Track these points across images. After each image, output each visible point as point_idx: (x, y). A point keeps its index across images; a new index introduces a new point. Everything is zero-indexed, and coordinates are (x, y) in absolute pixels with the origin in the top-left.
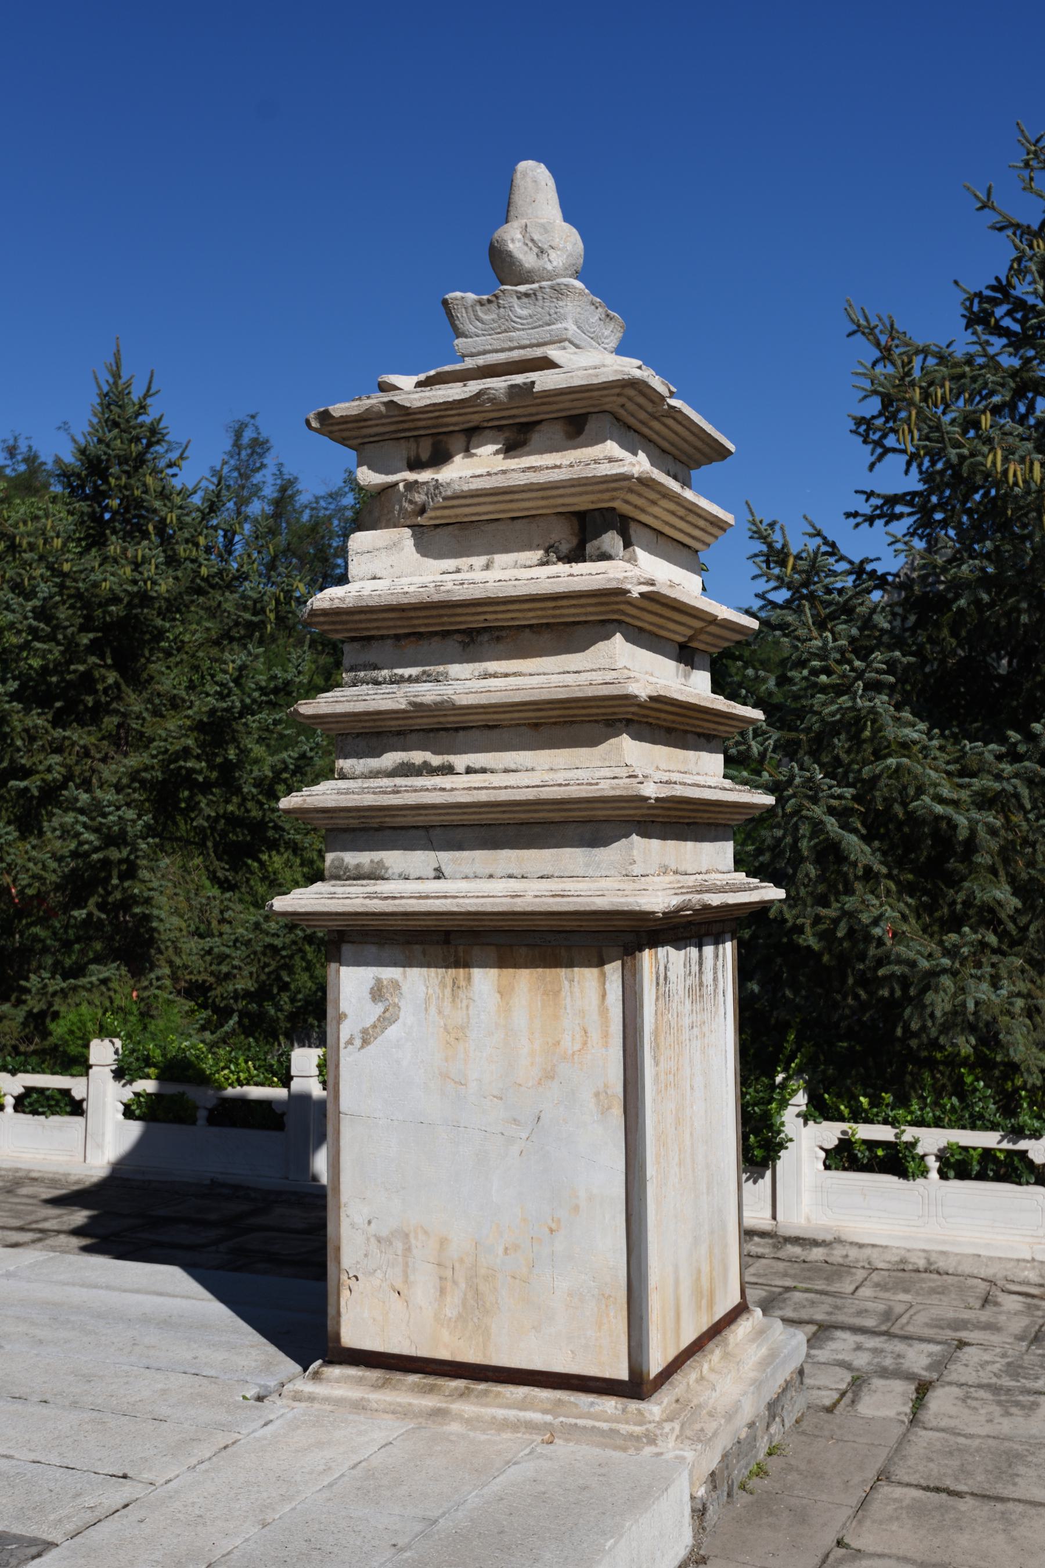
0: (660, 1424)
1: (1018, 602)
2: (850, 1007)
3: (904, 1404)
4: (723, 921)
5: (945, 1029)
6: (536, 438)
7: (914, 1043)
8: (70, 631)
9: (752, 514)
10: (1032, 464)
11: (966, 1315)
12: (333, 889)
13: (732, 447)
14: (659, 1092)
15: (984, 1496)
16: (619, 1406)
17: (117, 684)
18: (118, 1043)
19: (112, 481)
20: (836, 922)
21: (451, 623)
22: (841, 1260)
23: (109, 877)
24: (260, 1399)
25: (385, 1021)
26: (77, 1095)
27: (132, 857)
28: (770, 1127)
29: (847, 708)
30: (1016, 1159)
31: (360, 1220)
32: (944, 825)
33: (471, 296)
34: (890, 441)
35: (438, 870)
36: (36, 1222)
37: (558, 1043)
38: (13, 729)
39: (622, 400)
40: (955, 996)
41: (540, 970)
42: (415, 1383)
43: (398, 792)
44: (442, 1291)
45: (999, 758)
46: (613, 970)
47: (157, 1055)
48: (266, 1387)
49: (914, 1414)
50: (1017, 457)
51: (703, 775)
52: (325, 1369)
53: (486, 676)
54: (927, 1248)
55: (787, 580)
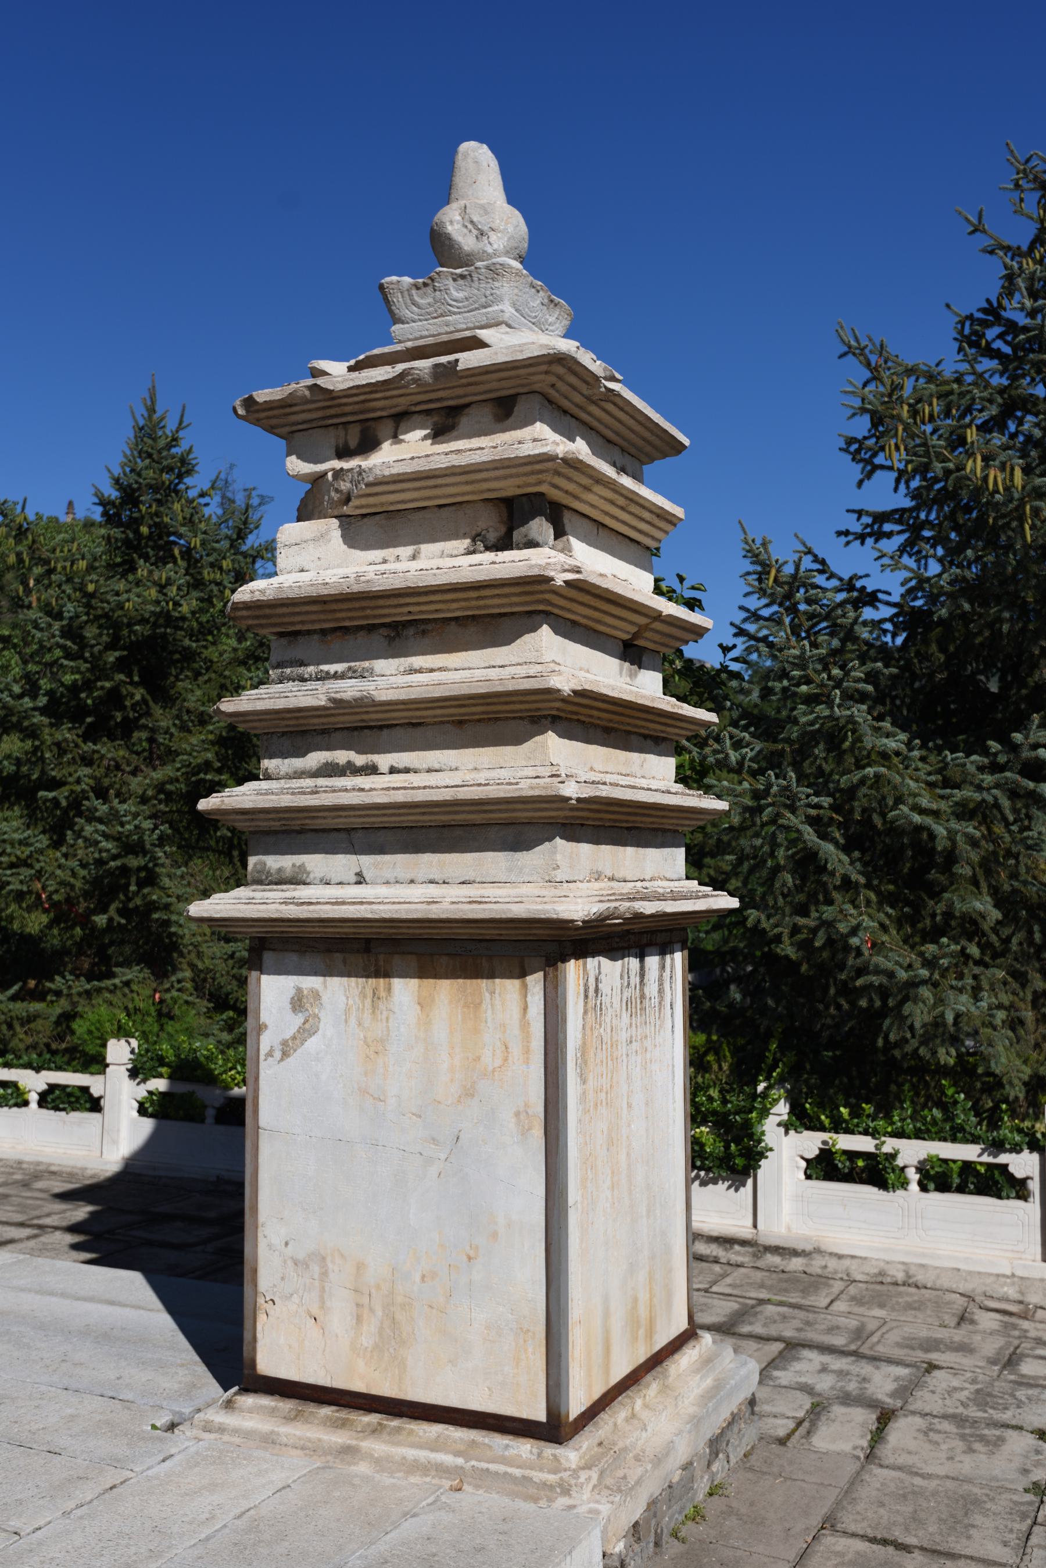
0: (575, 1473)
1: (1000, 611)
2: (833, 1017)
3: (862, 1437)
4: (671, 930)
5: (925, 1040)
6: (464, 422)
7: (897, 1053)
8: (96, 649)
9: (745, 533)
10: (1012, 469)
11: (941, 1334)
12: (252, 894)
13: (686, 441)
14: (586, 1111)
15: (934, 1552)
16: (535, 1451)
17: (144, 700)
18: (134, 1043)
19: (143, 508)
20: (814, 931)
21: (375, 617)
22: (819, 1271)
23: (128, 885)
24: (172, 1427)
25: (305, 1032)
26: (95, 1092)
27: (151, 865)
28: (751, 1136)
29: (825, 717)
30: (996, 1173)
31: (277, 1241)
32: (925, 836)
33: (407, 280)
34: (880, 459)
35: (359, 874)
36: (39, 1217)
37: (478, 1059)
38: (43, 743)
39: (552, 379)
40: (935, 1006)
41: (461, 981)
42: (327, 1417)
43: (317, 792)
44: (359, 1319)
45: (981, 769)
46: (535, 981)
47: (171, 1057)
48: (181, 1414)
49: (872, 1448)
50: (997, 463)
51: (650, 777)
52: (238, 1397)
53: (412, 671)
54: (906, 1260)
55: (769, 591)
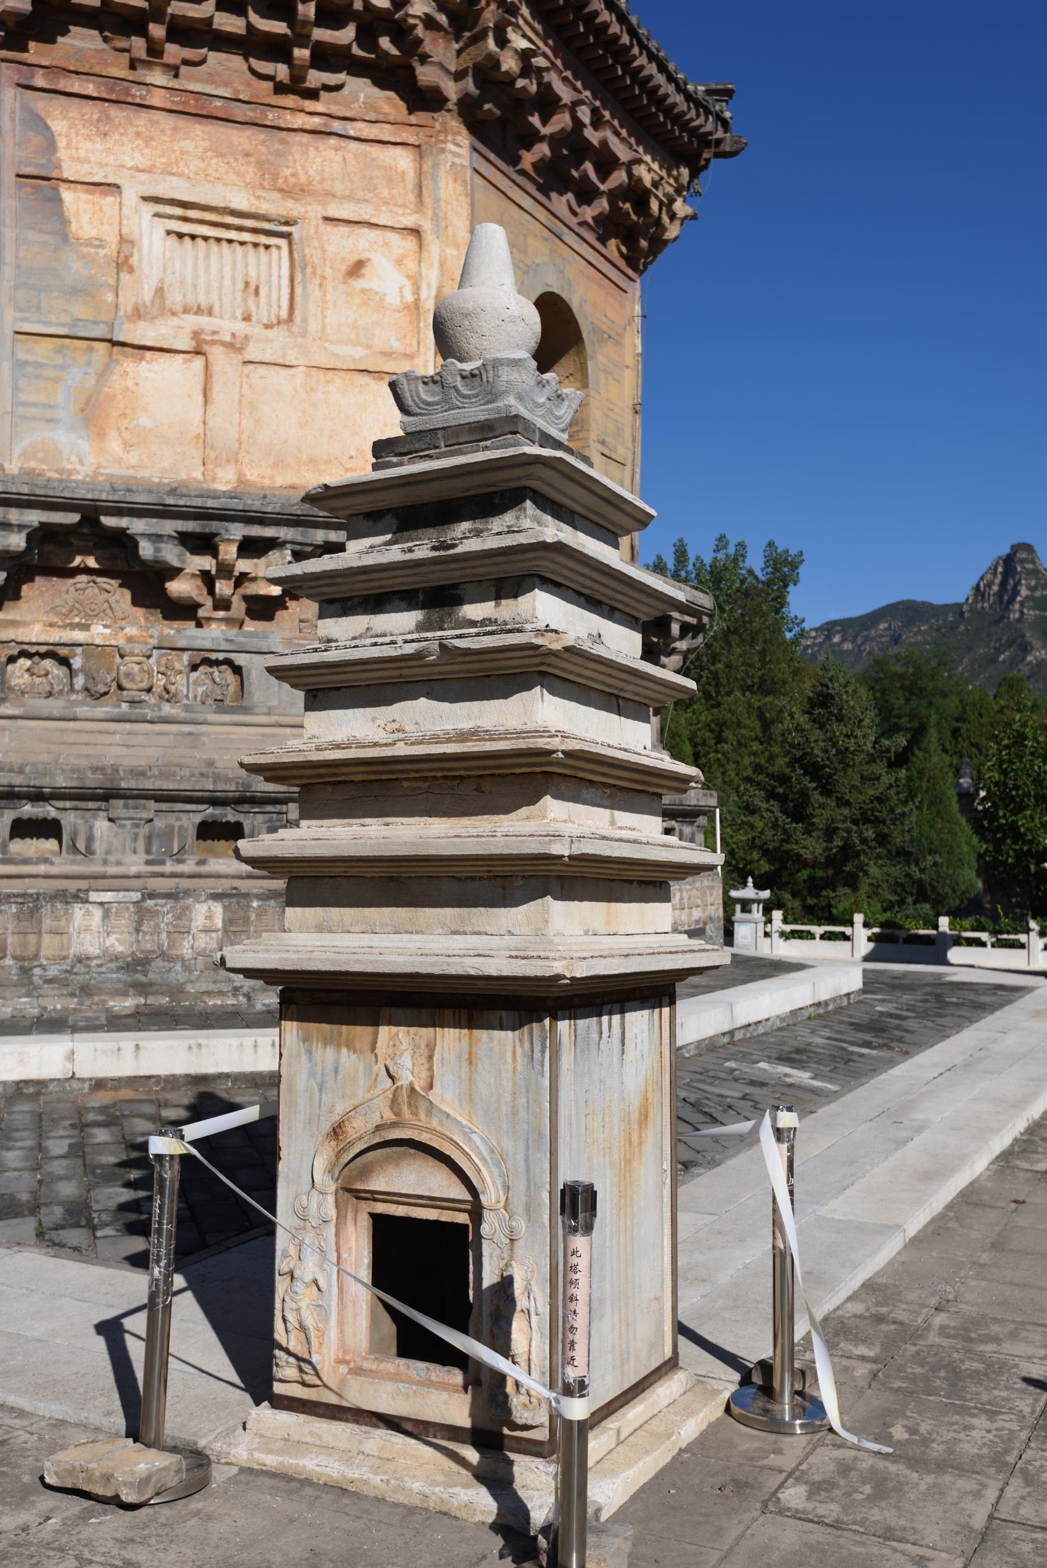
13: (652, 512)
